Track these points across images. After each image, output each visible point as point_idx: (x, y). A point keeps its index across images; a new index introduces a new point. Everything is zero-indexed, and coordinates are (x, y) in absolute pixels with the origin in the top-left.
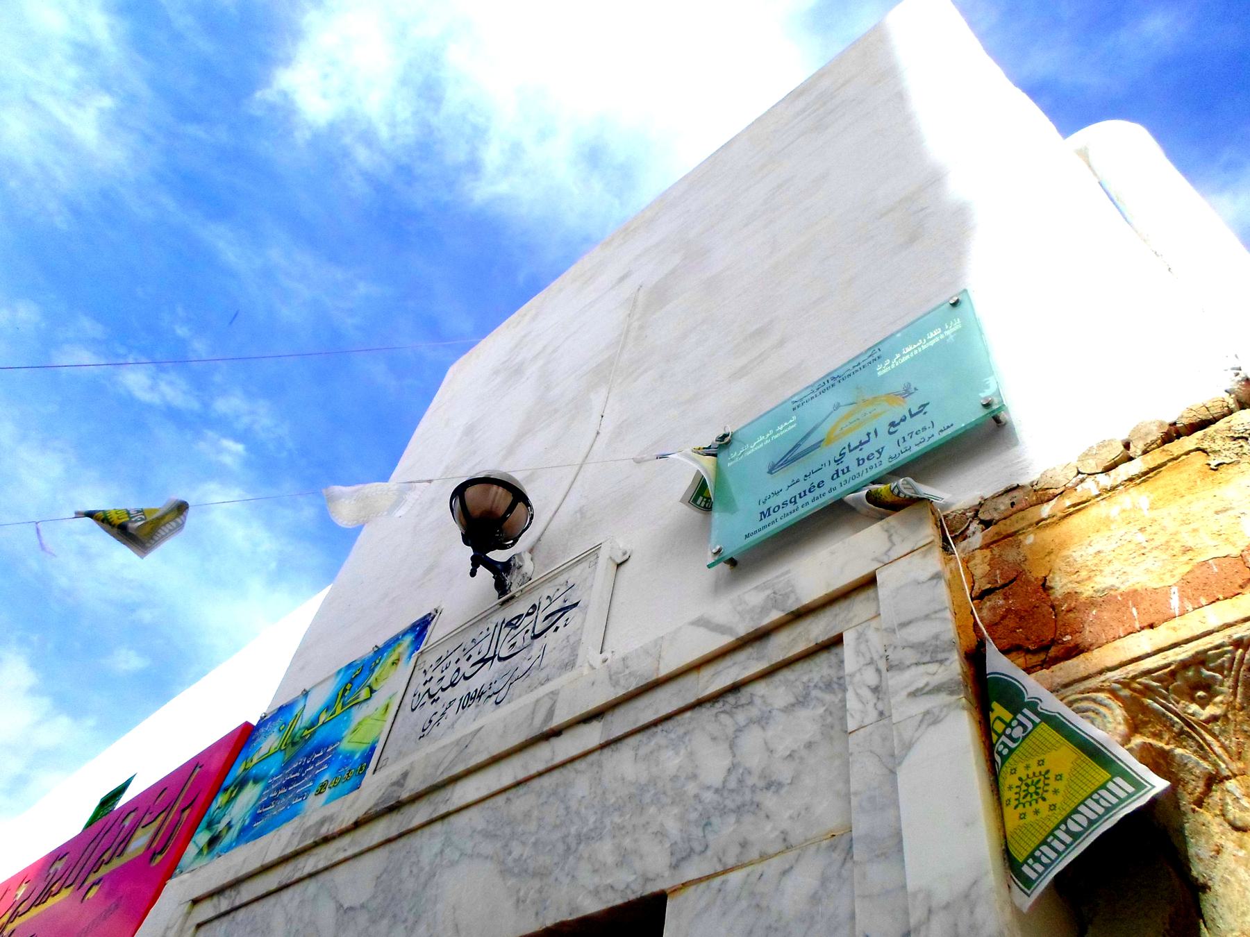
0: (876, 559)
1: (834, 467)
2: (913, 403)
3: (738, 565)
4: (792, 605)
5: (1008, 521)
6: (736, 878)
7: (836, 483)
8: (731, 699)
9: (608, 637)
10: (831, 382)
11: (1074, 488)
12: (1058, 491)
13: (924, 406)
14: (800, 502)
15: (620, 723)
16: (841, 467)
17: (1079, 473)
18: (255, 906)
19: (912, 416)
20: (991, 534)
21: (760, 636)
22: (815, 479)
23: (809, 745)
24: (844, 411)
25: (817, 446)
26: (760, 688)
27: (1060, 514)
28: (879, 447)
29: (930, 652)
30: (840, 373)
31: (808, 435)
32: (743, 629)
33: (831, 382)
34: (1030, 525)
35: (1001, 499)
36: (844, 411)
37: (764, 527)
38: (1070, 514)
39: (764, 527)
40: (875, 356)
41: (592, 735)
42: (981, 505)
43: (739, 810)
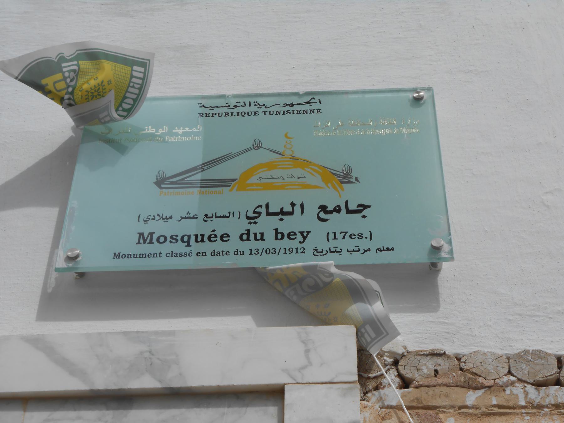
0: (286, 371)
1: (244, 225)
2: (353, 195)
3: (83, 288)
4: (175, 381)
5: (431, 391)
7: (245, 246)
9: (315, 381)
10: (254, 108)
11: (503, 387)
12: (487, 383)
13: (366, 207)
14: (195, 247)
16: (254, 229)
17: (510, 373)
19: (232, 115)
20: (128, 350)
22: (221, 227)
24: (262, 156)
27: (484, 409)
28: (305, 229)
30: (268, 101)
32: (102, 381)
33: (254, 108)
34: (452, 407)
35: (424, 360)
36: (262, 156)
37: (143, 256)
38: (494, 414)
39: (143, 256)
40: (315, 107)
42: (403, 356)
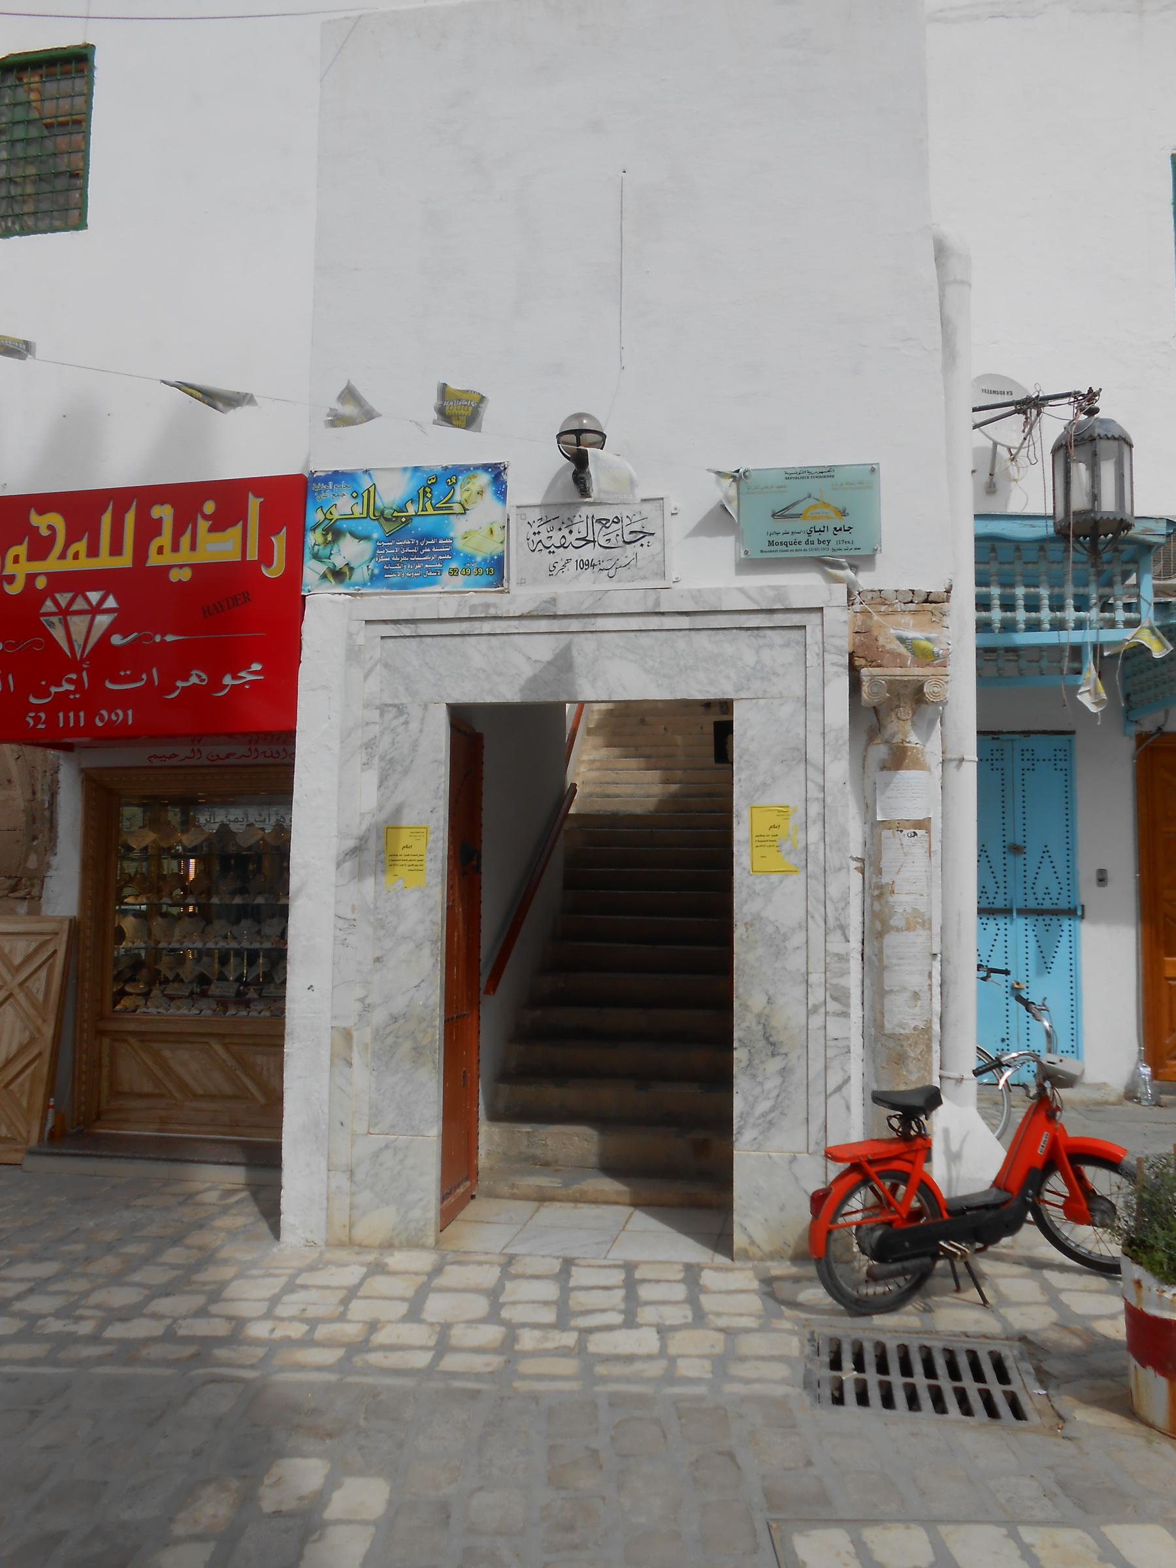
6: (762, 702)
8: (755, 632)
15: (700, 622)
18: (439, 639)
21: (771, 611)
23: (790, 664)
25: (798, 516)
26: (769, 633)
29: (839, 651)
31: (794, 505)
41: (684, 622)
43: (762, 678)
